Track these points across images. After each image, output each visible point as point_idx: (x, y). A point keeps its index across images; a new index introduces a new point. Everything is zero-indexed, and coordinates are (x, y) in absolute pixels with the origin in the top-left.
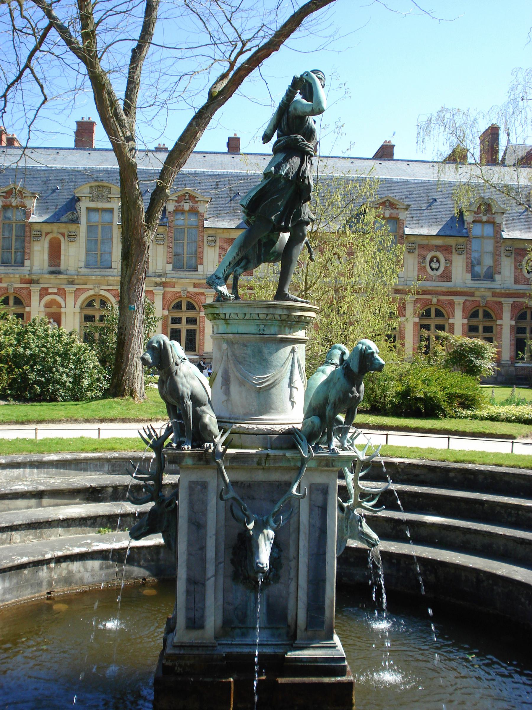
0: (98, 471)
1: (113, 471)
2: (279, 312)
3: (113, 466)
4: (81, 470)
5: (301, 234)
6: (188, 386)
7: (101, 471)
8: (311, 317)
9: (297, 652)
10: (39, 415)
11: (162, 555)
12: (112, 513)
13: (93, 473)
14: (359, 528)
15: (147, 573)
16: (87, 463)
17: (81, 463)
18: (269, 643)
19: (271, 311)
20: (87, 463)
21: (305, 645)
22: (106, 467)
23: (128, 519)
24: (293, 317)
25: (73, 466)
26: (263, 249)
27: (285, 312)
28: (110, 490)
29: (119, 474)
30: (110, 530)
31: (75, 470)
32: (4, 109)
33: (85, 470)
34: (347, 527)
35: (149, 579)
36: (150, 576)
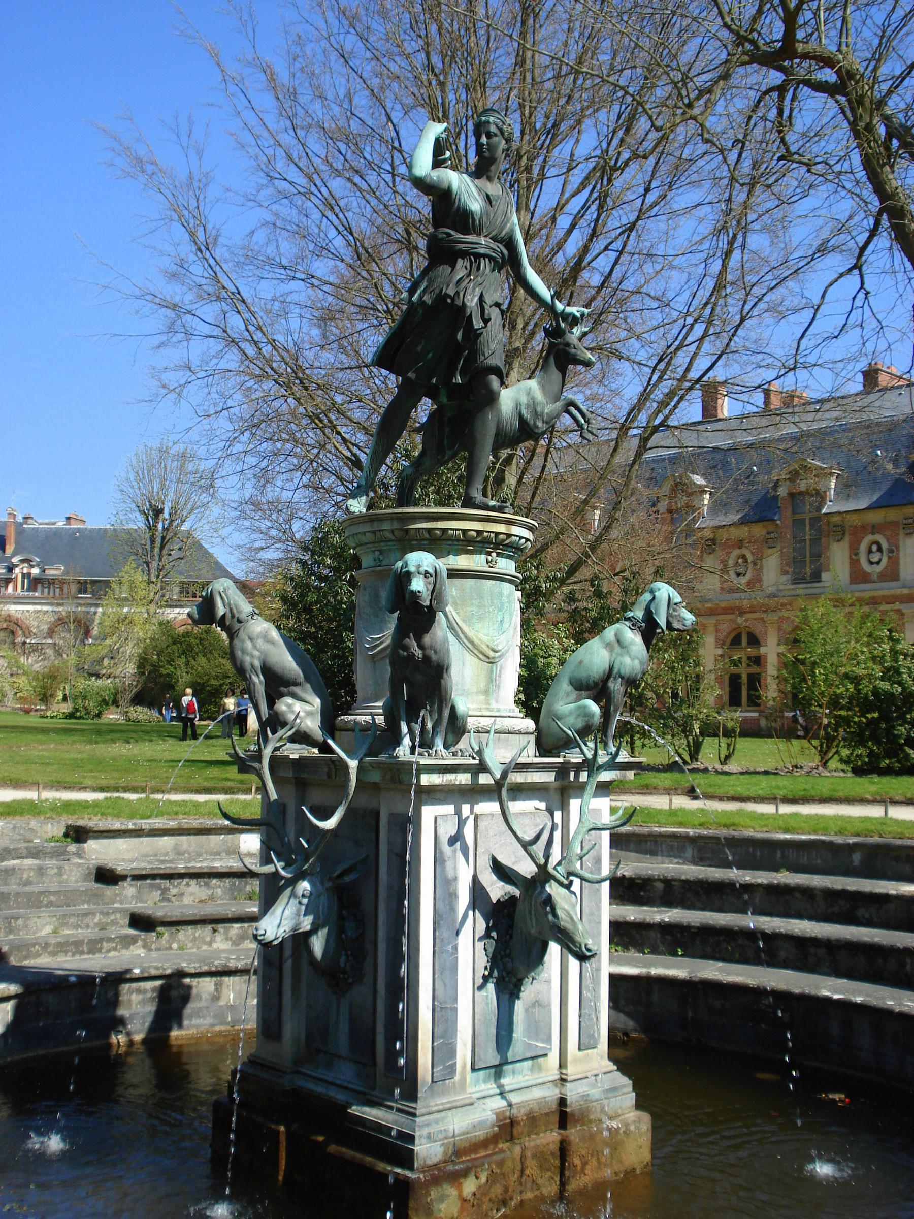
0: (675, 857)
1: (700, 860)
2: (386, 526)
3: (700, 850)
4: (646, 853)
5: (484, 391)
6: (256, 653)
7: (680, 857)
8: (521, 538)
9: (366, 1109)
10: (830, 790)
11: (655, 997)
12: (621, 920)
13: (667, 860)
14: (550, 917)
15: (631, 1024)
16: (656, 842)
17: (646, 841)
18: (350, 1086)
19: (376, 526)
20: (656, 842)
21: (378, 1100)
22: (689, 852)
23: (652, 934)
24: (412, 532)
25: (632, 846)
26: (447, 430)
27: (396, 525)
28: (660, 886)
29: (711, 866)
30: (619, 948)
31: (637, 852)
32: (862, 287)
33: (653, 853)
34: (530, 913)
35: (634, 1035)
36: (636, 1030)
